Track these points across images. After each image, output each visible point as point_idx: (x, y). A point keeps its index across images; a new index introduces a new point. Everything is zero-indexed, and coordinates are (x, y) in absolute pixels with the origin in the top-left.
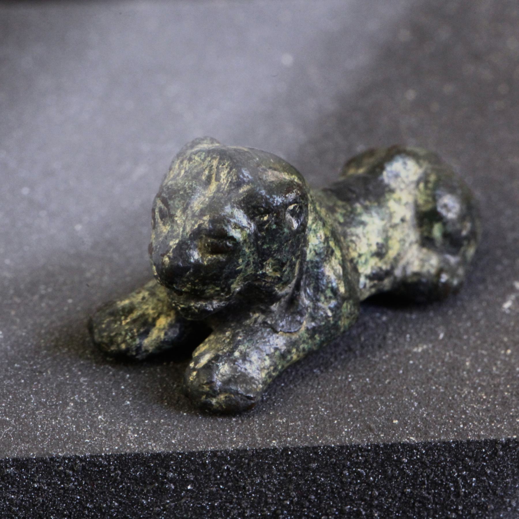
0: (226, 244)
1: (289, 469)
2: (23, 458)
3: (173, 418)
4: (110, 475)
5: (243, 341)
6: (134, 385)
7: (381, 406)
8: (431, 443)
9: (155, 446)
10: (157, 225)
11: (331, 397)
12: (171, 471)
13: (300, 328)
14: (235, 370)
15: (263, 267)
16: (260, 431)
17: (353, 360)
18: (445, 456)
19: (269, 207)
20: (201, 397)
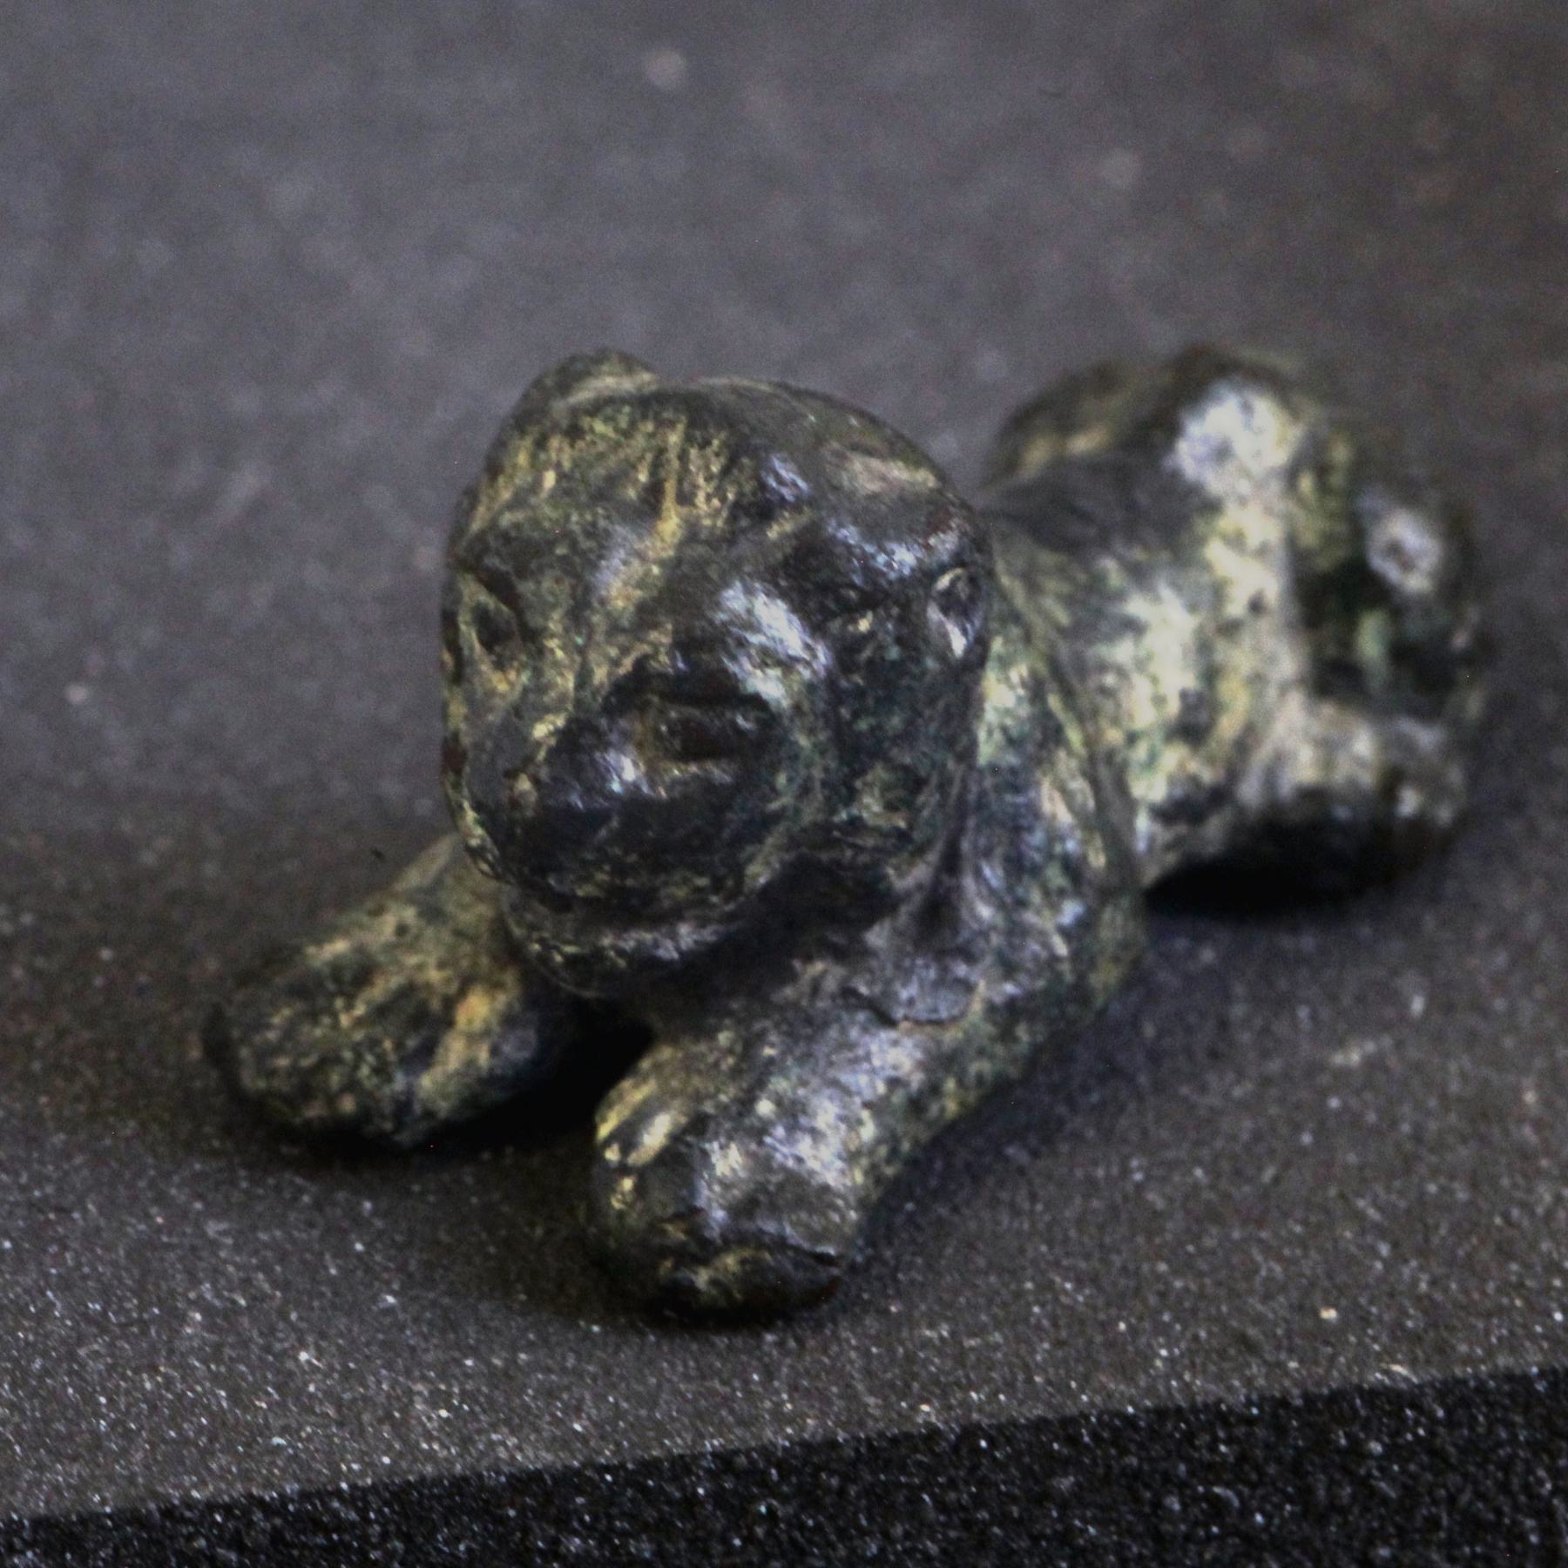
0: (734, 725)
1: (978, 1501)
2: (67, 1517)
3: (558, 1344)
4: (367, 1558)
5: (783, 1060)
6: (399, 1238)
7: (1266, 1260)
8: (1464, 1382)
9: (520, 1448)
10: (468, 670)
11: (1086, 1239)
12: (576, 1533)
13: (968, 1005)
14: (762, 1163)
15: (852, 796)
16: (868, 1373)
17: (1132, 1106)
18: (1509, 1426)
19: (875, 584)
20: (655, 1267)
